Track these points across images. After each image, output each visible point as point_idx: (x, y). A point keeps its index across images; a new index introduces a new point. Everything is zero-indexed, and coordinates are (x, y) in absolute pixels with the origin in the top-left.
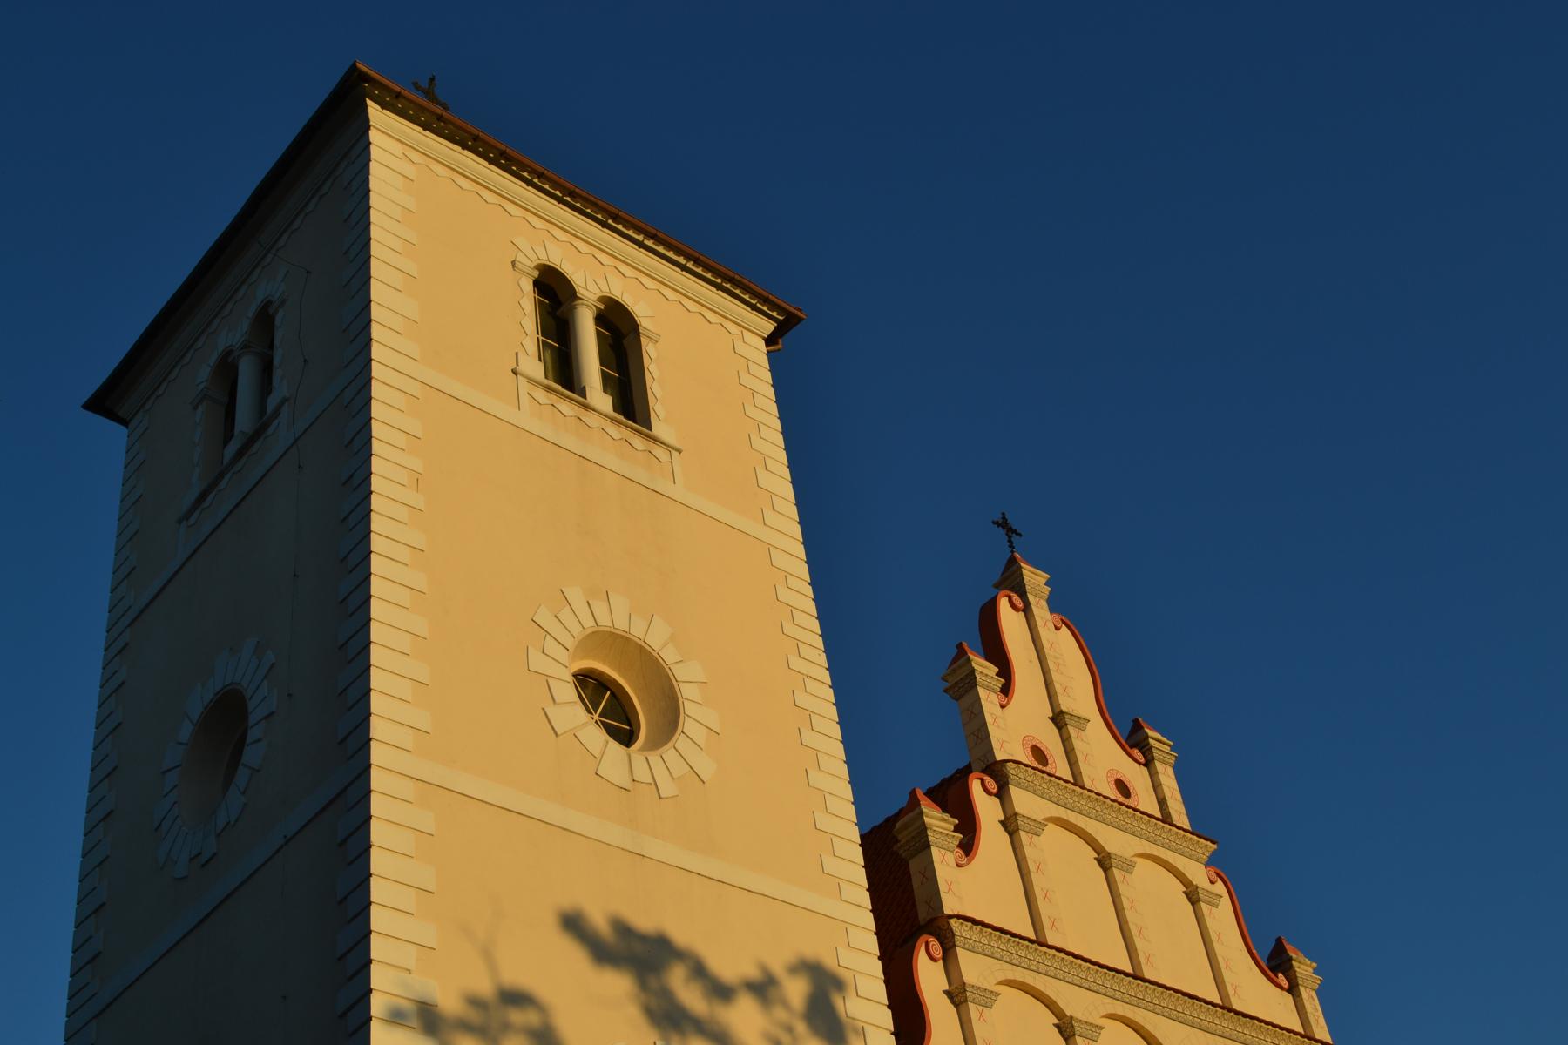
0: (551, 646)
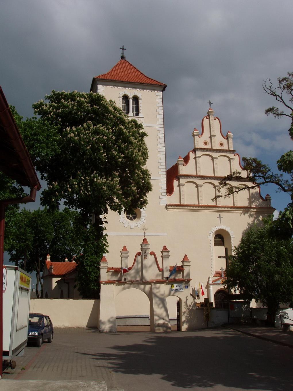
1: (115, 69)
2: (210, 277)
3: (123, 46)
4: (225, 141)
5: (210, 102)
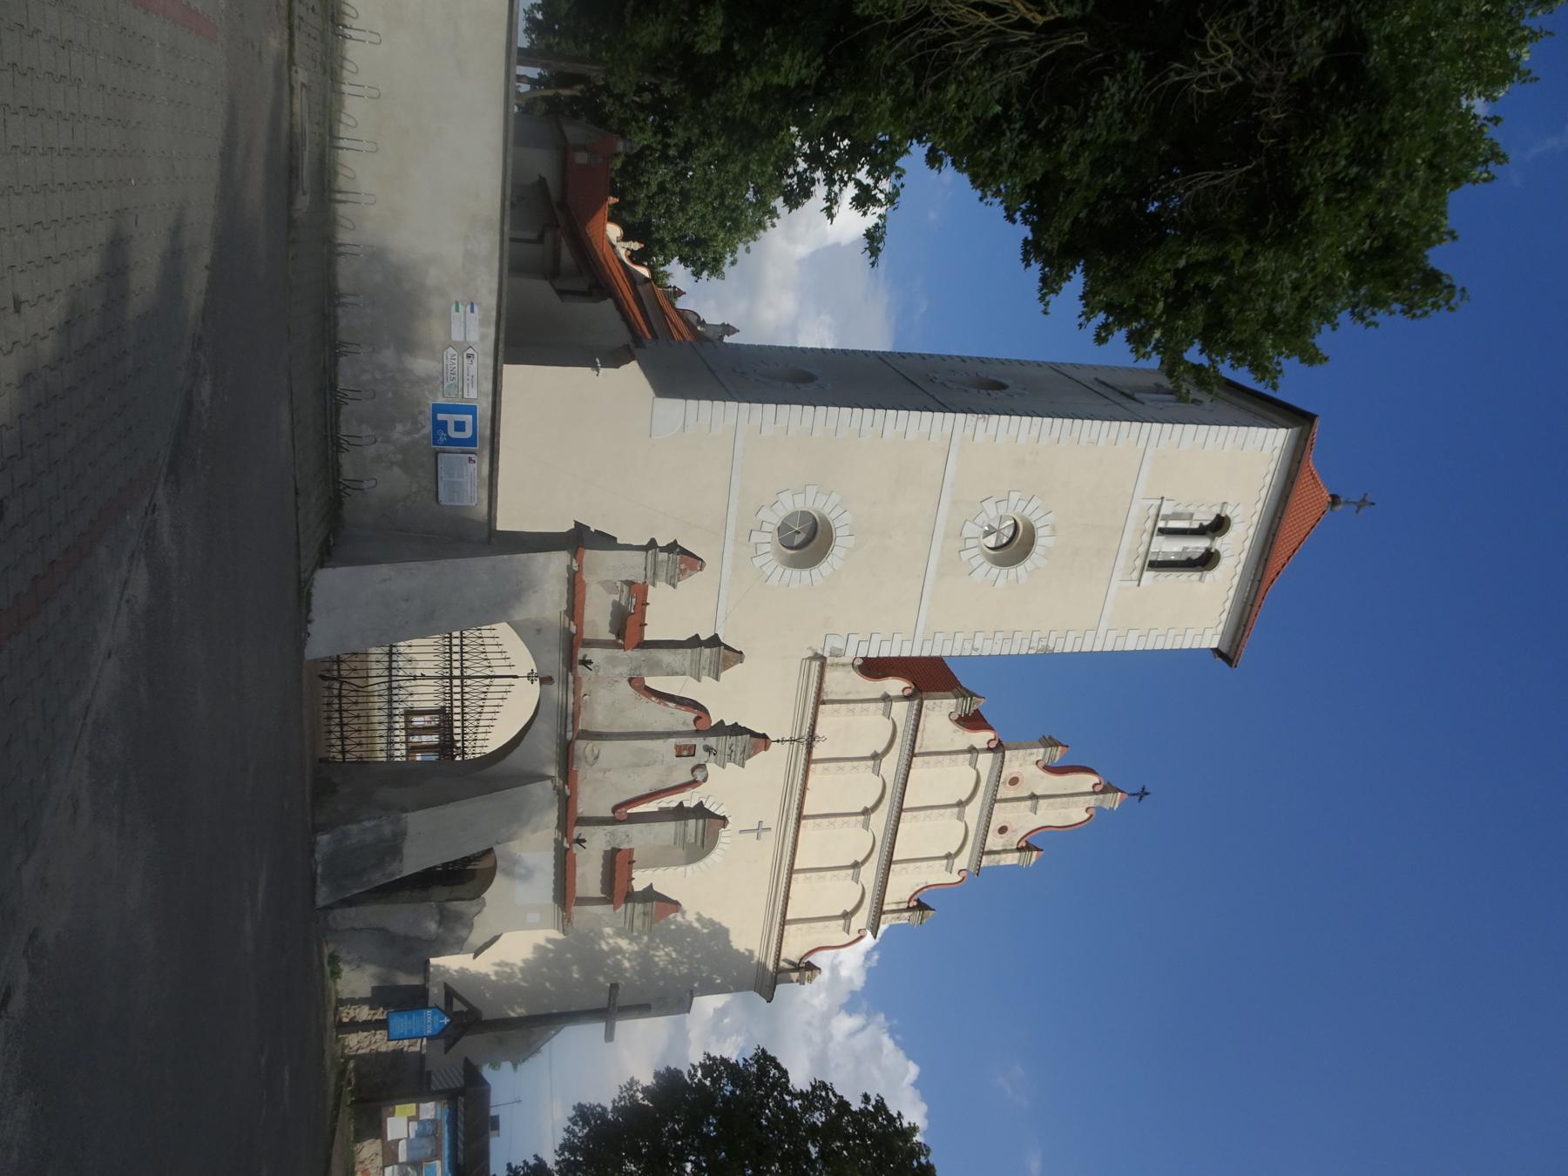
0: (1022, 504)
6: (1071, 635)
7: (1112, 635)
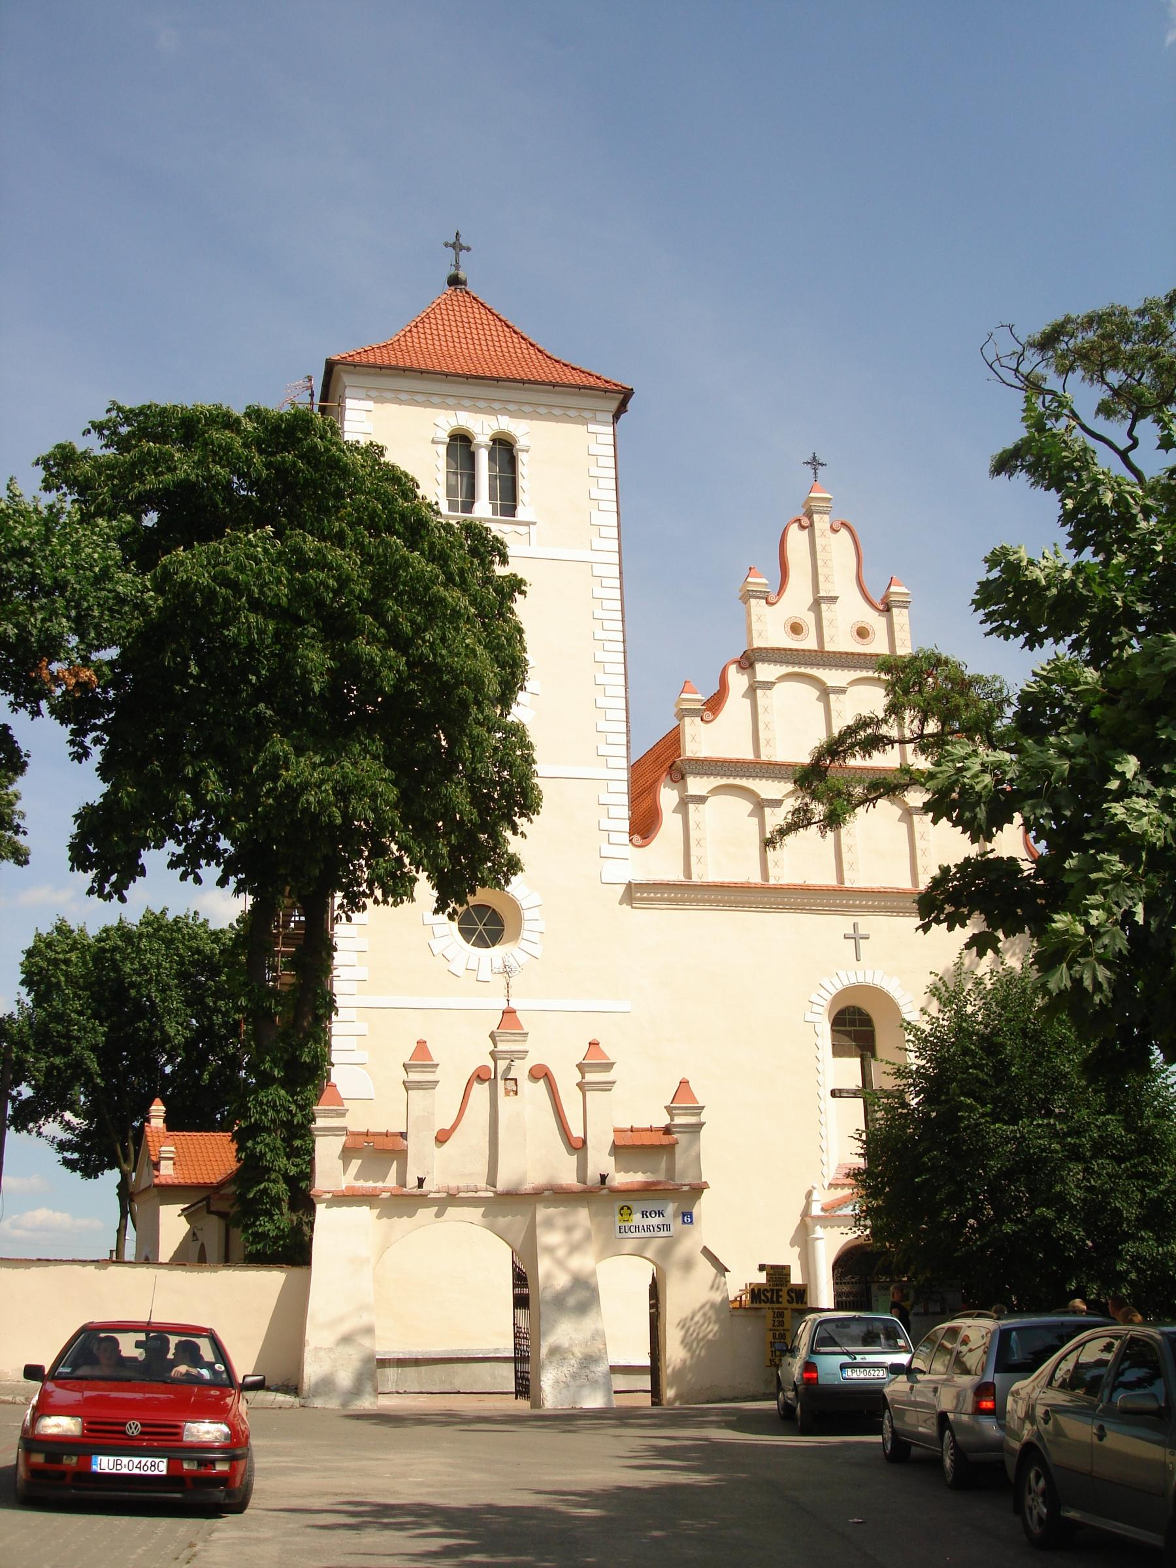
1: (420, 325)
2: (814, 1188)
3: (457, 234)
4: (877, 623)
5: (814, 458)
6: (599, 592)
7: (598, 544)
